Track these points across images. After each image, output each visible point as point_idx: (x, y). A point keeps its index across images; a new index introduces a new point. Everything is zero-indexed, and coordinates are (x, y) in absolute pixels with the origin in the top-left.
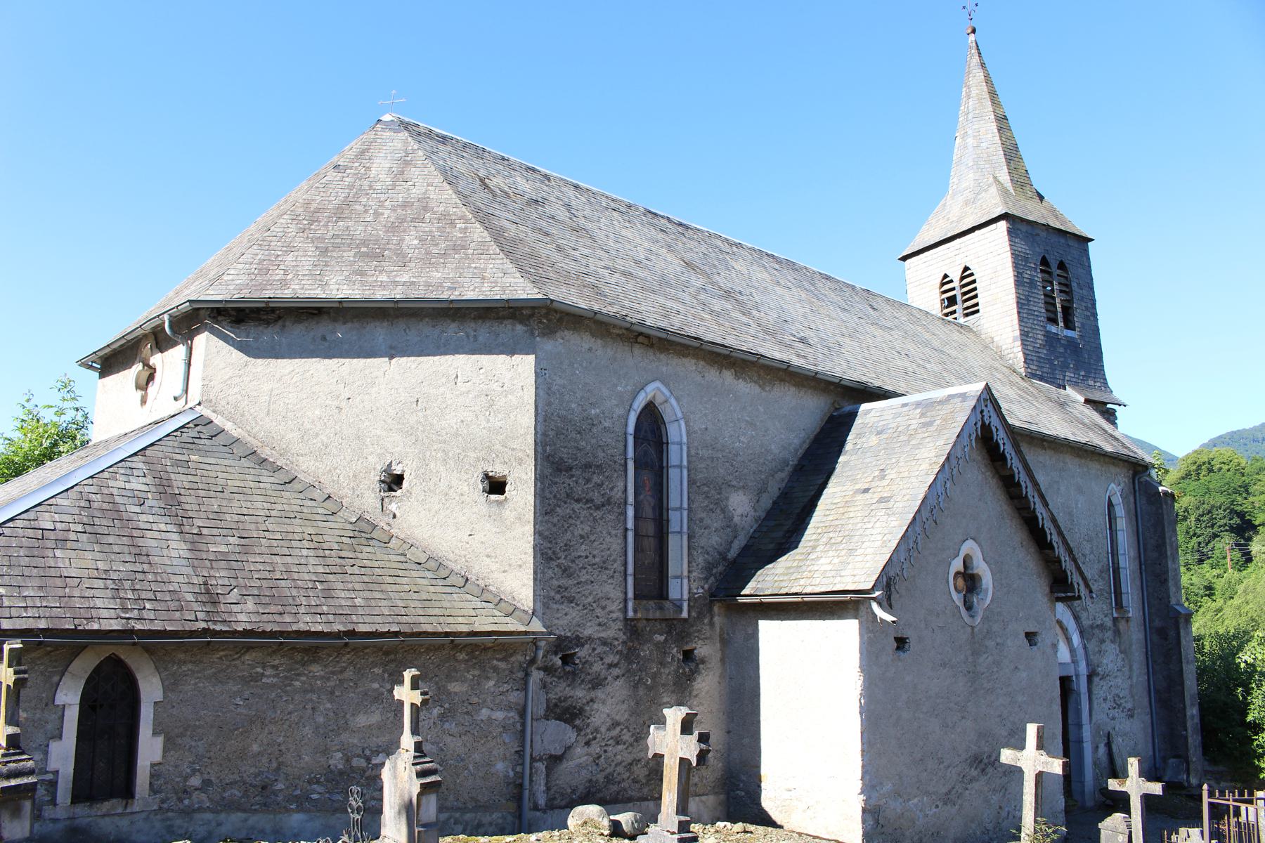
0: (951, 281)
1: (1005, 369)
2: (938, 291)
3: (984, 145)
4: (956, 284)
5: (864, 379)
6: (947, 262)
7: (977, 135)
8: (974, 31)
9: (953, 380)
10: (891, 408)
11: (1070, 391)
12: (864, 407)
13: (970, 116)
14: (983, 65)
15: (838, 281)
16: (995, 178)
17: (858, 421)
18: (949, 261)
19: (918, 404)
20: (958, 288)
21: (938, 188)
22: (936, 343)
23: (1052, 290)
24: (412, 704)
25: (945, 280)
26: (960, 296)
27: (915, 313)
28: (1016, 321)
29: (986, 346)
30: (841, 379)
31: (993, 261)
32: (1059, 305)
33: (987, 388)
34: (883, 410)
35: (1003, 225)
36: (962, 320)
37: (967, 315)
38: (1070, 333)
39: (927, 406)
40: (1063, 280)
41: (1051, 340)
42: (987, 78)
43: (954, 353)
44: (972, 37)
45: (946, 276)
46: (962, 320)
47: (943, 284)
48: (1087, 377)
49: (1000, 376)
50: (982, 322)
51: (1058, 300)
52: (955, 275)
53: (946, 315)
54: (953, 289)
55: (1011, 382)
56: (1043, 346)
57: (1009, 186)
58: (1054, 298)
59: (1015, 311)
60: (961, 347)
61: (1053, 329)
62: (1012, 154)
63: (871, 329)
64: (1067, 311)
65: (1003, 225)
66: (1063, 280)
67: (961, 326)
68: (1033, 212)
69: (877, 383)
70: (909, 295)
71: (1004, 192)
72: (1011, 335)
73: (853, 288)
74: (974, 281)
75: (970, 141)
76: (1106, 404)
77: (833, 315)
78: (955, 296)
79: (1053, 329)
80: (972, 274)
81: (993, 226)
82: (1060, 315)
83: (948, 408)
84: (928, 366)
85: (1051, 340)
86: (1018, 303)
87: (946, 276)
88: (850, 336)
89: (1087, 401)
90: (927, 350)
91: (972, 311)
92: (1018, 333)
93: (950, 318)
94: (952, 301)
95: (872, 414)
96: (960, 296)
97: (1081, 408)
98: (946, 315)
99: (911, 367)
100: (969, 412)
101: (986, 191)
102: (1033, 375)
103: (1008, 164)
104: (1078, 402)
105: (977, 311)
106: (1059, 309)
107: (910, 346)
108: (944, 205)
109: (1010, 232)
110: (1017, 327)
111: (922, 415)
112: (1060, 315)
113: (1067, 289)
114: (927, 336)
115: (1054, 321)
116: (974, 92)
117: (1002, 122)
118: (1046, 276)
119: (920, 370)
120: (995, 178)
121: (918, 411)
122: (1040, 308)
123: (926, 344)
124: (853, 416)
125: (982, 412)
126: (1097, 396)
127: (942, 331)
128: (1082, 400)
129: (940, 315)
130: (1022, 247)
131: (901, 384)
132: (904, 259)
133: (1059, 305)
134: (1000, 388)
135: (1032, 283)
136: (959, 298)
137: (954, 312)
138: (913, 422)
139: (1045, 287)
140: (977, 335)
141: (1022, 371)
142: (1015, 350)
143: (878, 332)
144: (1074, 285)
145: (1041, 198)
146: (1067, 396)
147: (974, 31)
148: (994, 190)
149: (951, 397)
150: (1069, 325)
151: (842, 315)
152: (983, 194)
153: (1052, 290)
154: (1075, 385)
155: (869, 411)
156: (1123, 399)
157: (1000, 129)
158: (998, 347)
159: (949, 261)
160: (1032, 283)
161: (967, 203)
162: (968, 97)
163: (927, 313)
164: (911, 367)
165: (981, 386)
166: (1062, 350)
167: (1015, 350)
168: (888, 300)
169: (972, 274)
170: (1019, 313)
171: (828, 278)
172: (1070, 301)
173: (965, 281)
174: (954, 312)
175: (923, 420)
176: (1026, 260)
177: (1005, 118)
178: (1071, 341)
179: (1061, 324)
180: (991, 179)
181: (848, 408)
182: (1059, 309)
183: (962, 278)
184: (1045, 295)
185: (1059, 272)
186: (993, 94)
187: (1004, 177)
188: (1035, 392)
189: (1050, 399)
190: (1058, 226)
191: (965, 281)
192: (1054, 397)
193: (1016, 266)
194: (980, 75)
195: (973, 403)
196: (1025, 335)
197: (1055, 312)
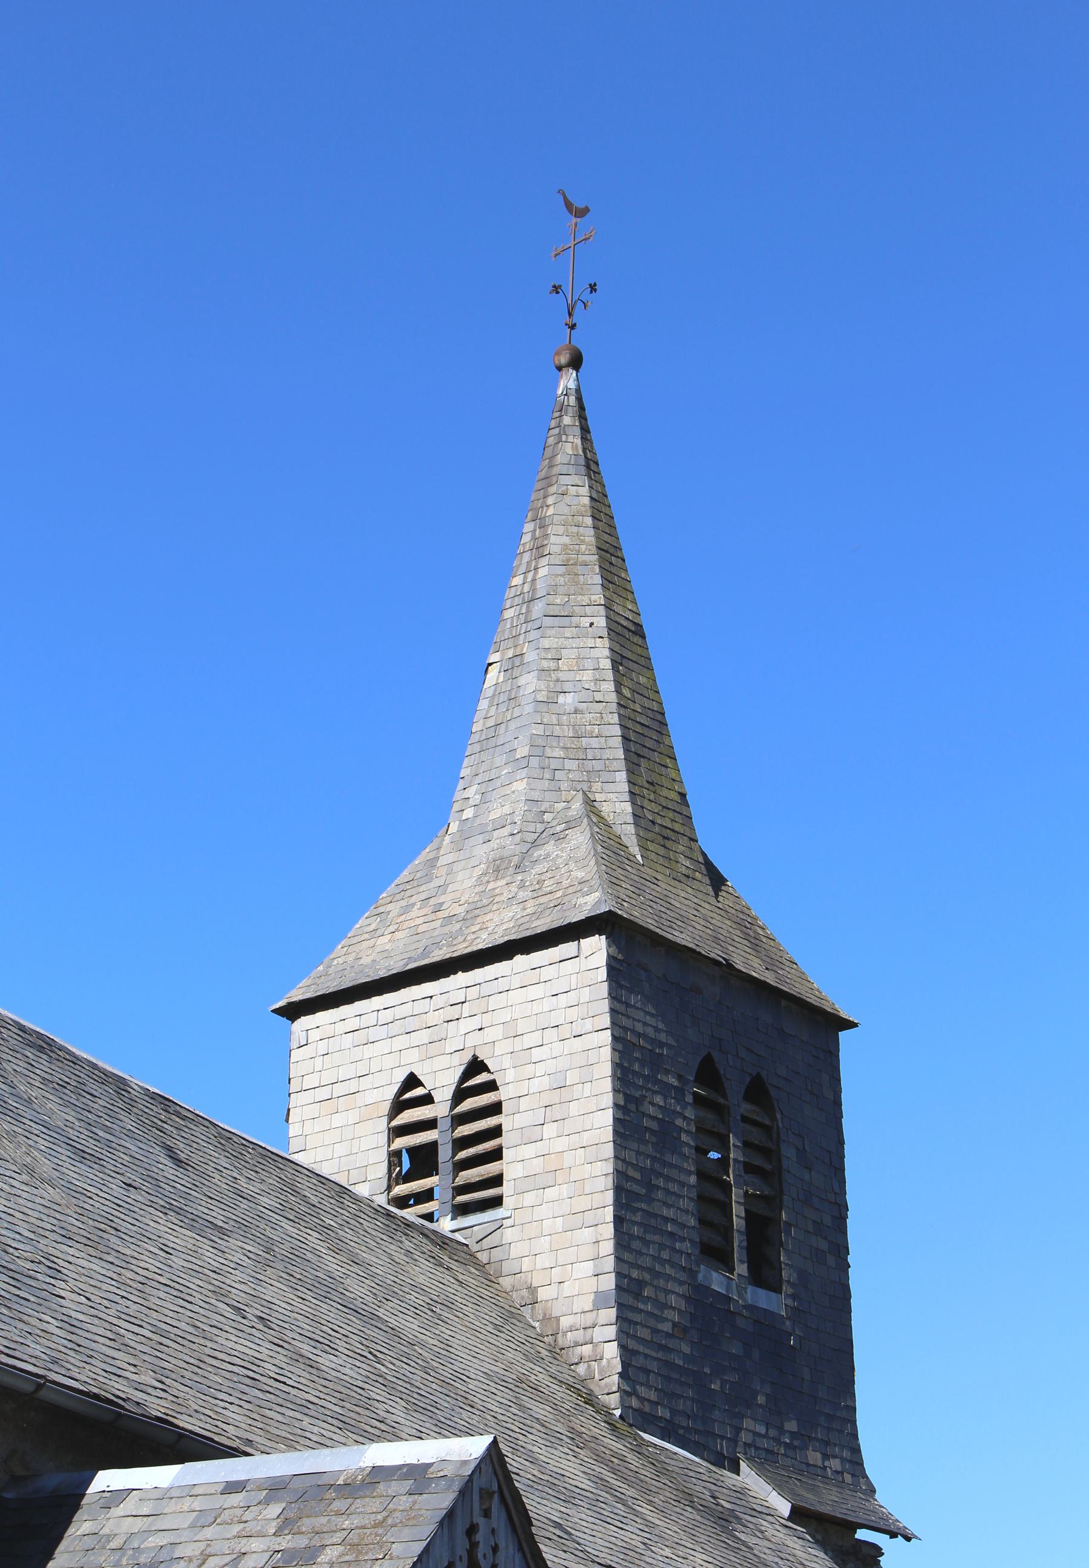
0: (427, 1099)
1: (561, 1393)
2: (383, 1124)
3: (567, 701)
4: (440, 1109)
5: (118, 1388)
6: (424, 1036)
7: (547, 668)
8: (576, 362)
9: (399, 1414)
10: (190, 1491)
11: (749, 1478)
12: (107, 1479)
13: (538, 608)
14: (591, 466)
15: (75, 1060)
16: (590, 804)
17: (81, 1527)
18: (417, 1038)
19: (276, 1488)
20: (444, 1124)
21: (424, 811)
22: (358, 1289)
23: (724, 1162)
24: (500, 1125)
25: (410, 1092)
26: (451, 1146)
27: (306, 1187)
28: (608, 1247)
29: (513, 1312)
30: (41, 1383)
31: (553, 1043)
32: (738, 1211)
33: (494, 1452)
34: (163, 1495)
35: (595, 949)
36: (446, 1225)
37: (462, 1210)
38: (762, 1298)
39: (302, 1496)
40: (756, 1136)
41: (707, 1310)
42: (600, 508)
43: (410, 1326)
44: (568, 380)
45: (412, 1081)
46: (446, 1225)
47: (399, 1106)
48: (803, 1439)
49: (541, 1411)
50: (509, 1235)
51: (736, 1194)
52: (441, 1081)
53: (402, 1202)
54: (430, 1124)
55: (575, 1434)
56: (681, 1331)
57: (628, 833)
58: (726, 1187)
59: (609, 1213)
60: (435, 1309)
61: (717, 1282)
62: (646, 740)
63: (161, 1226)
64: (761, 1228)
65: (595, 949)
66: (756, 1136)
67: (443, 1242)
68: (688, 921)
69: (156, 1406)
70: (294, 1130)
71: (608, 845)
72: (592, 1285)
73: (120, 1085)
74: (496, 1109)
75: (529, 683)
76: (855, 1526)
77: (45, 1167)
78: (433, 1146)
79: (717, 1282)
80: (492, 1086)
81: (567, 949)
82: (738, 1241)
83: (368, 1508)
84: (325, 1361)
85: (707, 1310)
86: (618, 1189)
87: (476, 1066)
88: (89, 1243)
89: (799, 1515)
90: (329, 1313)
91: (482, 1198)
92: (609, 1282)
93: (409, 1214)
94: (424, 1160)
95: (129, 1506)
96: (451, 1146)
97: (780, 1535)
98: (402, 1202)
99: (272, 1361)
100: (428, 1529)
101: (558, 837)
102: (638, 1418)
103: (632, 768)
104: (769, 1513)
105: (496, 1202)
106: (738, 1223)
107: (276, 1292)
108: (432, 863)
109: (615, 971)
110: (610, 1263)
111: (286, 1525)
112: (738, 1241)
113: (764, 1165)
114: (332, 1264)
115: (720, 1257)
116: (557, 540)
117: (628, 642)
118: (710, 1117)
119: (298, 1374)
120: (590, 804)
121: (274, 1510)
122: (682, 1212)
123: (328, 1290)
124: (67, 1504)
125: (472, 1530)
126: (829, 1501)
127: (383, 1255)
128: (784, 1508)
129: (381, 1200)
130: (647, 1022)
131: (234, 1414)
132: (293, 1011)
133: (738, 1211)
134: (542, 1452)
135: (667, 1135)
136: (444, 1153)
137: (427, 1196)
138: (256, 1544)
139: (702, 1151)
140: (488, 1275)
141: (613, 1400)
142: (599, 1334)
143: (183, 1239)
144: (788, 1153)
145: (717, 881)
146: (742, 1493)
147: (576, 362)
148: (580, 839)
149: (379, 1474)
150: (763, 1273)
151: (78, 1174)
152: (550, 847)
153: (724, 1162)
154: (766, 1463)
155: (121, 1495)
156: (905, 1519)
157: (618, 662)
158: (547, 1319)
159: (417, 1038)
160: (667, 1135)
161: (497, 867)
162: (539, 550)
163: (343, 1191)
164: (272, 1361)
165: (475, 1447)
166: (736, 1349)
167: (599, 1334)
168: (225, 1138)
169: (492, 1086)
170: (618, 1220)
171: (44, 1045)
172: (773, 1201)
173: (470, 1104)
174: (427, 1196)
175: (285, 1542)
176: (655, 1062)
177: (638, 631)
178: (763, 1319)
179: (741, 1269)
180: (577, 806)
181: (53, 1480)
182: (738, 1223)
183: (460, 1094)
184: (701, 1175)
185: (746, 1108)
186: (610, 556)
187: (617, 806)
188: (647, 1472)
189: (689, 1499)
190: (756, 968)
191: (470, 1104)
192: (699, 1489)
193: (623, 1076)
194: (581, 494)
195: (446, 1500)
196: (631, 1294)
197: (727, 1230)
